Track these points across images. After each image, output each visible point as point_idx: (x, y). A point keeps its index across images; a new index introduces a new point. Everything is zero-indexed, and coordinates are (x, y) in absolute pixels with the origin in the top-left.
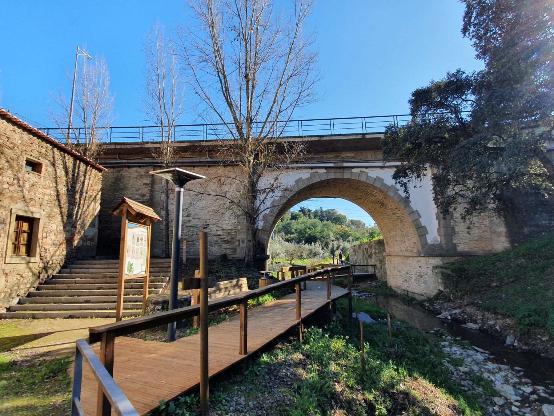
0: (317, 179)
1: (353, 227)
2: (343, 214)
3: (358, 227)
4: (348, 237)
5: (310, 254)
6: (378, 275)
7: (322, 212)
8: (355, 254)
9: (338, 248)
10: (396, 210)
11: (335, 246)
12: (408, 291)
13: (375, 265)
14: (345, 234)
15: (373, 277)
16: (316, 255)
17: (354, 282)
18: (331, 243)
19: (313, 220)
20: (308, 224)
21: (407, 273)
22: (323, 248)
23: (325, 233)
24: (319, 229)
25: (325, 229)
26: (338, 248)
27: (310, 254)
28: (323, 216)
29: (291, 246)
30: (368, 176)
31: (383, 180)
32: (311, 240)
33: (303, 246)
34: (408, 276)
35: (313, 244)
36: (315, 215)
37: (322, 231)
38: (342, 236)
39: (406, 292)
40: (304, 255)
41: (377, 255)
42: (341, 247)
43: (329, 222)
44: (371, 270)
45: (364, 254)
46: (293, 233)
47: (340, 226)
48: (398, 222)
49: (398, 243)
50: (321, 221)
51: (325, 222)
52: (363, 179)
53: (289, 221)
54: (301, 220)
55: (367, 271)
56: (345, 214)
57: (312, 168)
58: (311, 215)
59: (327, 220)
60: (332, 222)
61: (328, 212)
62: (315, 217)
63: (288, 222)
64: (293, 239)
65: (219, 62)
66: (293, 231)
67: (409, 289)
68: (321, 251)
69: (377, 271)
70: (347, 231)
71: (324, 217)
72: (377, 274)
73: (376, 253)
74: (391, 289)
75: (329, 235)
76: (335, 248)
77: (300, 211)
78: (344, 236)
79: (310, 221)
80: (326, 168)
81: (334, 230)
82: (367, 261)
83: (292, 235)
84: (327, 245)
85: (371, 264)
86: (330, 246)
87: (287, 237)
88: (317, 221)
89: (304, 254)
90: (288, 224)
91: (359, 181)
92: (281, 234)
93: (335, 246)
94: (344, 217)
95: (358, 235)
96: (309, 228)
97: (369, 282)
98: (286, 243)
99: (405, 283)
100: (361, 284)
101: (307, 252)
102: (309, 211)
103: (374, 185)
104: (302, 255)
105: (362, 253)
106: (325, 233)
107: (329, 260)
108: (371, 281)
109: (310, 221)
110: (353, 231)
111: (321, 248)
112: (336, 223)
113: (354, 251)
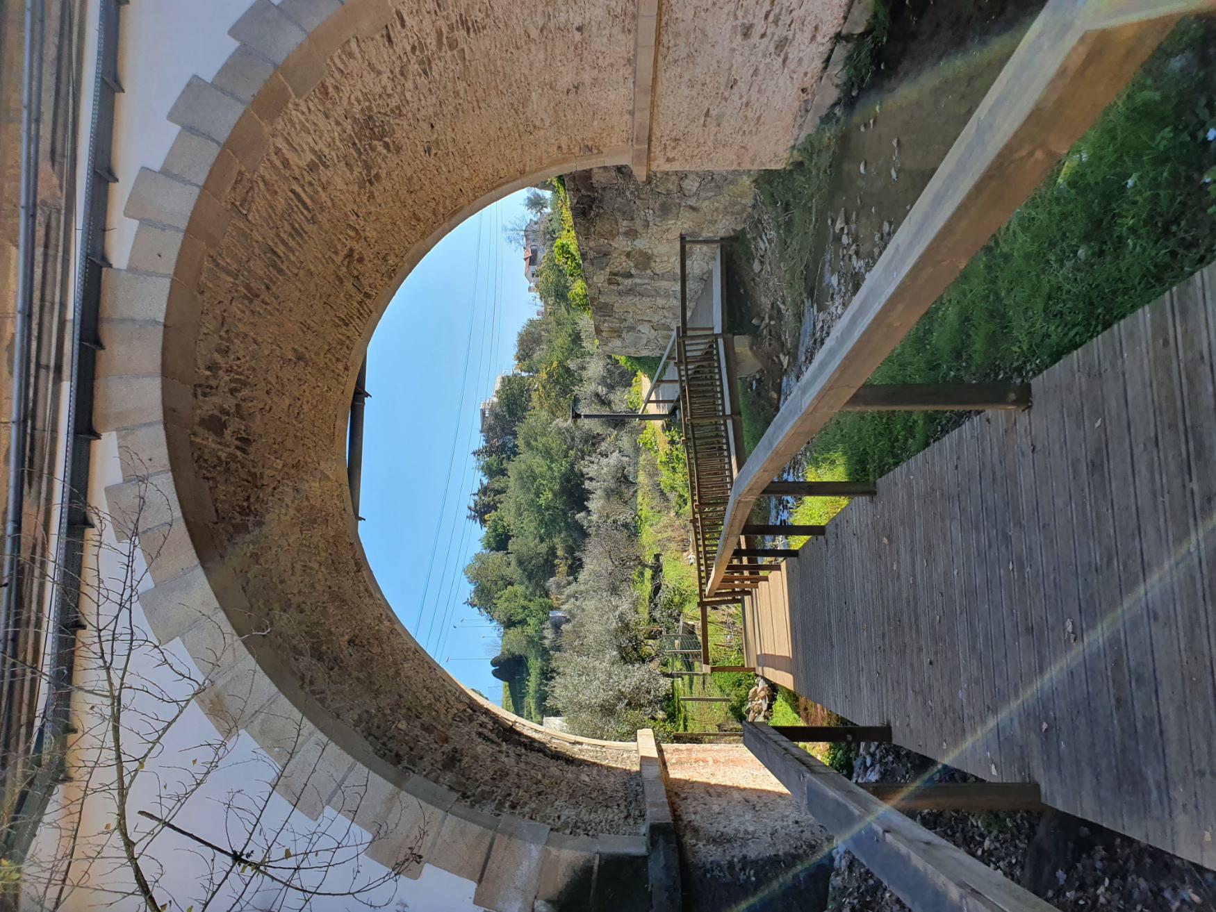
0: (163, 494)
1: (536, 356)
2: (498, 386)
3: (537, 341)
4: (568, 370)
5: (620, 495)
6: (724, 226)
7: (488, 451)
8: (631, 329)
9: (604, 402)
10: (403, 44)
11: (596, 409)
12: (838, 37)
13: (682, 238)
14: (557, 382)
15: (734, 254)
16: (626, 477)
17: (754, 332)
18: (586, 424)
19: (512, 482)
20: (524, 499)
21: (747, 33)
22: (605, 455)
23: (555, 444)
24: (539, 464)
25: (540, 442)
26: (604, 402)
27: (620, 495)
28: (502, 449)
29: (595, 562)
30: (165, 172)
31: (195, 85)
32: (574, 492)
33: (594, 518)
34: (759, 27)
35: (587, 485)
36: (494, 472)
37: (547, 454)
38: (565, 391)
39: (840, 52)
40: (625, 516)
41: (638, 225)
42: (602, 390)
43: (521, 429)
44: (706, 262)
45: (630, 291)
46: (552, 550)
47: (534, 396)
48: (475, 45)
49: (587, 76)
50: (515, 454)
51: (520, 442)
52: (179, 203)
53: (512, 558)
54: (509, 519)
55: (706, 280)
56: (499, 380)
57: (78, 522)
58: (496, 486)
59: (514, 434)
60: (521, 419)
61: (488, 430)
62: (503, 472)
63: (514, 563)
64: (570, 551)
65: (22, 738)
66: (543, 548)
67: (830, 28)
68: (614, 458)
69: (705, 235)
70: (550, 375)
71: (504, 445)
72: (722, 233)
73: (632, 234)
74: (810, 148)
75: (559, 432)
76: (605, 411)
77: (483, 522)
78: (565, 380)
79: (515, 494)
80: (85, 430)
81: (544, 415)
82: (661, 277)
83: (560, 553)
84: (593, 440)
85: (675, 261)
86: (596, 427)
87: (563, 568)
88: (513, 467)
89: (621, 518)
90: (520, 563)
91: (194, 230)
92: (553, 589)
93: (596, 409)
94: (507, 381)
95: (562, 340)
96: (537, 495)
97: (756, 266)
98: (582, 576)
99: (793, 54)
100: (765, 301)
101: (616, 505)
102: (484, 491)
103: (223, 134)
104: (626, 526)
105: (629, 299)
106: (555, 444)
107: (647, 435)
108: (750, 259)
109: (515, 494)
110: (549, 356)
111: (604, 461)
112: (525, 409)
113: (617, 333)
